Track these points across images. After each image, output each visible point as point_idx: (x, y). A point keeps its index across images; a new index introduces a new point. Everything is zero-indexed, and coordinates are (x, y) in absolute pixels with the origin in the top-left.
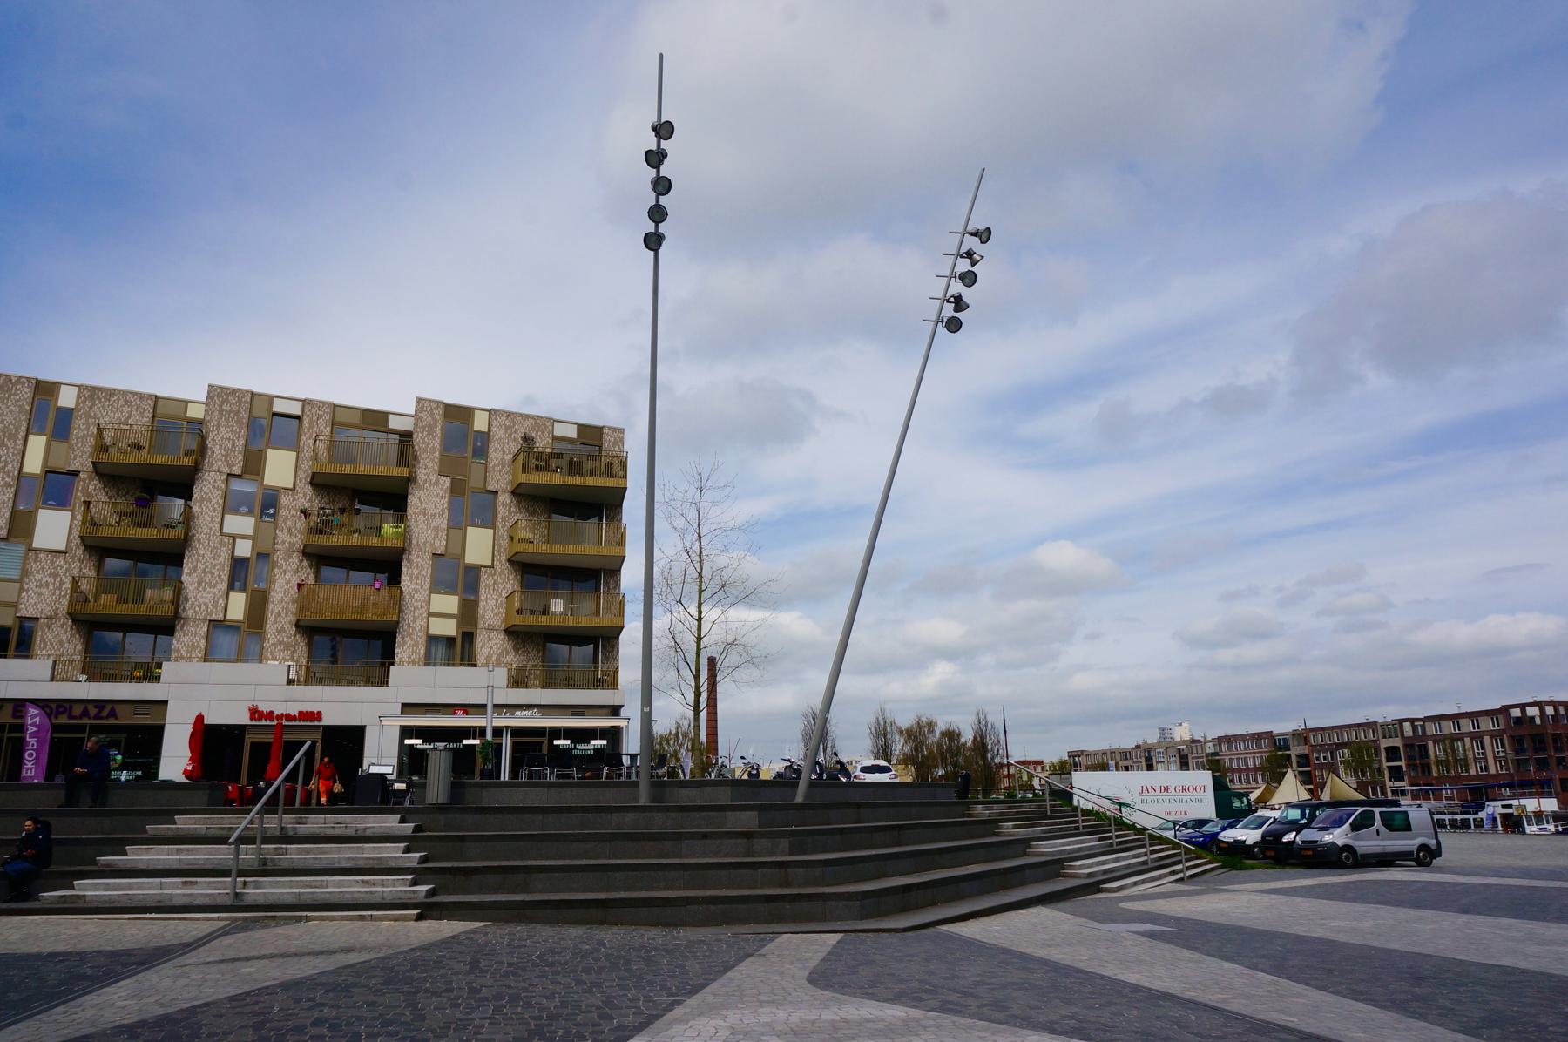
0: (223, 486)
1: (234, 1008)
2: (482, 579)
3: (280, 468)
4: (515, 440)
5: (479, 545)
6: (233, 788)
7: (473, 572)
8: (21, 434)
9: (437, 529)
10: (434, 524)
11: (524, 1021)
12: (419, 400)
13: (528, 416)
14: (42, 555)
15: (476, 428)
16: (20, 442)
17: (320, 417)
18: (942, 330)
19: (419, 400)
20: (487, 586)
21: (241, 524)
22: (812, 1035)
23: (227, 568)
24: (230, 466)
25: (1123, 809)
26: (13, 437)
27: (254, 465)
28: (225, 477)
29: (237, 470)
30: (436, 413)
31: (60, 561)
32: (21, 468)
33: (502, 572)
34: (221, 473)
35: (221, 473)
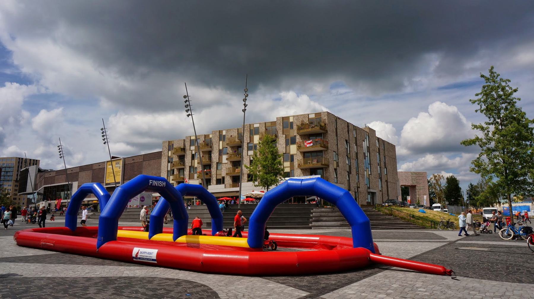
0: (247, 146)
1: (426, 261)
2: (294, 157)
3: (256, 139)
4: (299, 122)
5: (293, 149)
6: (453, 199)
7: (292, 157)
8: (218, 142)
9: (283, 147)
10: (283, 146)
11: (16, 289)
12: (277, 118)
13: (302, 115)
14: (224, 164)
15: (314, 117)
16: (218, 143)
17: (263, 126)
18: (186, 95)
19: (277, 118)
20: (296, 159)
21: (251, 153)
22: (269, 297)
23: (249, 162)
24: (248, 141)
25: (227, 229)
26: (217, 143)
27: (251, 139)
28: (247, 144)
29: (249, 142)
30: (281, 120)
31: (227, 165)
32: (219, 148)
33: (299, 155)
34: (246, 143)
35: (246, 143)
